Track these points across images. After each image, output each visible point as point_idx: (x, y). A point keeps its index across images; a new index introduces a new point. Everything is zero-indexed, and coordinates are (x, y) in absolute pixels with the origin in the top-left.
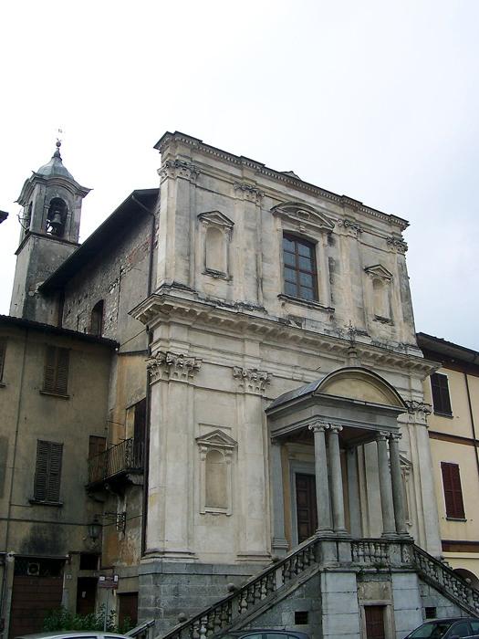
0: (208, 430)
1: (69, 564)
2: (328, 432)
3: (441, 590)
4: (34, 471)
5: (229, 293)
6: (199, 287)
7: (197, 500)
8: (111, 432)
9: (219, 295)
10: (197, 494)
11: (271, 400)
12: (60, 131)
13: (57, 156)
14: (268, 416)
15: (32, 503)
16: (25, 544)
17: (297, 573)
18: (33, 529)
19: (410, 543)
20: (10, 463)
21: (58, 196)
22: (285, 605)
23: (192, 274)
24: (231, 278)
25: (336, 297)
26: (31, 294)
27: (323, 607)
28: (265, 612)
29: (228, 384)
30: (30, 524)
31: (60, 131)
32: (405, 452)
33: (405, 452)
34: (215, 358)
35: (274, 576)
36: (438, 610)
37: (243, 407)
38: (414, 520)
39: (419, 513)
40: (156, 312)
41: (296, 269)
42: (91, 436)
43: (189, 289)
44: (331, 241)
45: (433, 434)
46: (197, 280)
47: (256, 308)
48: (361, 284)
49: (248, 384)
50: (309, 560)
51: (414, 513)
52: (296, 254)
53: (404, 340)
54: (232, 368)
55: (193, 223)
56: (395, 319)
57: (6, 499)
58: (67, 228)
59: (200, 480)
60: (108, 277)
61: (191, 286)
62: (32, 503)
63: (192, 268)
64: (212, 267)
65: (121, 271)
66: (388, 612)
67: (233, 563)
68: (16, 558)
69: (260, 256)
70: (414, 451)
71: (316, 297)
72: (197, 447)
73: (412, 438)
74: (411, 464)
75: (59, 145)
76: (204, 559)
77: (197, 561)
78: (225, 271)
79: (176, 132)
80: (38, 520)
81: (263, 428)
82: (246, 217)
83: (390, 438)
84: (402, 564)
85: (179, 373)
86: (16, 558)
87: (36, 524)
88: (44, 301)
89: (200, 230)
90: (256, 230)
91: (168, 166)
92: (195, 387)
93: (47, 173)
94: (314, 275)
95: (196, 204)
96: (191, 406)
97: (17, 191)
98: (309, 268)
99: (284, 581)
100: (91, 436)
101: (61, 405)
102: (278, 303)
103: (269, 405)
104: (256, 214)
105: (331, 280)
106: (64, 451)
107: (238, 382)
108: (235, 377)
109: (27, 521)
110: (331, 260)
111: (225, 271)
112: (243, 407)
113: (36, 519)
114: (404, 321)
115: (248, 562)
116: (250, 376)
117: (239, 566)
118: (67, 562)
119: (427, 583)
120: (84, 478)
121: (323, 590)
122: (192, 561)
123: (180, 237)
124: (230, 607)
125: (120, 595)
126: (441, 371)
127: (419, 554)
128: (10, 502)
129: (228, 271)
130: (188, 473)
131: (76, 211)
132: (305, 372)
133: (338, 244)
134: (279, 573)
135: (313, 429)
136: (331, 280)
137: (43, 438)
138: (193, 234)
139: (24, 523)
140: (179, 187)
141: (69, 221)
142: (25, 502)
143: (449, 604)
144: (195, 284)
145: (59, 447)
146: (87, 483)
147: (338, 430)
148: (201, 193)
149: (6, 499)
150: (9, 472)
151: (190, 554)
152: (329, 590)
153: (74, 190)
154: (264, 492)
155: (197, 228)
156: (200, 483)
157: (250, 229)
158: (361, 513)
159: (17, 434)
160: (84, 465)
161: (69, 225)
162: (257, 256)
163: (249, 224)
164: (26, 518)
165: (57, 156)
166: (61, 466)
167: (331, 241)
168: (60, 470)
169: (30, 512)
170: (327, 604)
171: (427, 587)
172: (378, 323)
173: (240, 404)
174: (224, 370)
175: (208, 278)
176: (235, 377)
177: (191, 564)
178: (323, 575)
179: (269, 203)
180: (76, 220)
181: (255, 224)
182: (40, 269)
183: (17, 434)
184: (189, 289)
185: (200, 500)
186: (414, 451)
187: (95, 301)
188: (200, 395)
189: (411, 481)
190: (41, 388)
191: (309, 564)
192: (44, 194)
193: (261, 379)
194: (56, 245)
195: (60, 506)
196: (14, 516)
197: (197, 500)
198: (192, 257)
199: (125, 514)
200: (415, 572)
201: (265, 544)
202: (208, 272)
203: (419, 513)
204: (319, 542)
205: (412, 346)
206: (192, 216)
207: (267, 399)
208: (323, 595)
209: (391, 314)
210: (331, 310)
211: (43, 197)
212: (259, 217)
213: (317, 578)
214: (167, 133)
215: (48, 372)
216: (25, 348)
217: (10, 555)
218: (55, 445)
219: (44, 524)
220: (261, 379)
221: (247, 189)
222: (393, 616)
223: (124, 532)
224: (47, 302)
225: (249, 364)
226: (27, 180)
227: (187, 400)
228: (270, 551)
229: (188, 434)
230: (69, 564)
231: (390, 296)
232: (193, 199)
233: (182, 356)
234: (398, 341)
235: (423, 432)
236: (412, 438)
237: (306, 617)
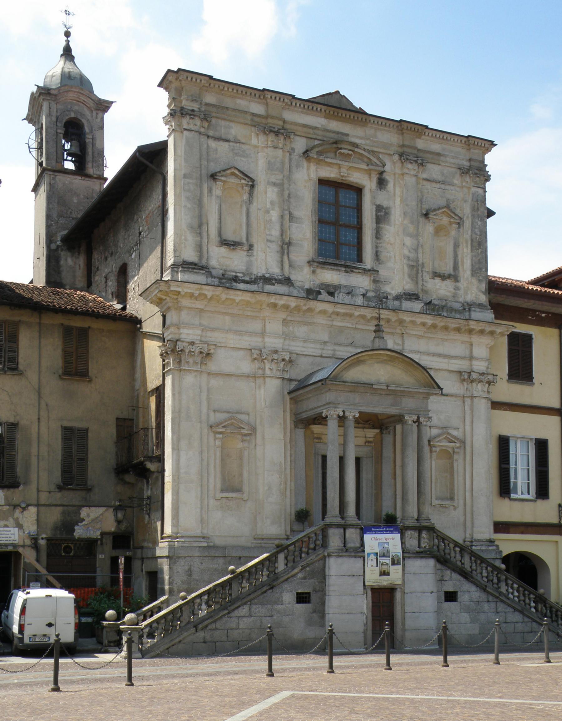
0: (221, 416)
1: (102, 544)
2: (342, 419)
3: (465, 575)
4: (59, 457)
5: (249, 265)
6: (213, 263)
7: (211, 487)
8: (137, 415)
9: (236, 269)
10: (212, 480)
11: (295, 380)
12: (67, 13)
13: (67, 53)
14: (291, 399)
15: (60, 488)
16: (56, 528)
17: (301, 557)
18: (63, 513)
19: (431, 529)
20: (34, 451)
21: (73, 115)
22: (286, 586)
23: (205, 248)
24: (251, 247)
25: (382, 256)
26: (53, 246)
27: (327, 588)
28: (265, 592)
29: (246, 367)
30: (60, 509)
31: (67, 13)
32: (456, 428)
33: (456, 428)
34: (233, 340)
35: (276, 561)
36: (459, 594)
37: (262, 391)
38: (461, 502)
39: (468, 494)
40: (164, 297)
41: (336, 224)
42: (117, 419)
43: (202, 268)
44: (382, 183)
45: (496, 405)
46: (211, 254)
47: (279, 282)
48: (416, 236)
49: (268, 366)
50: (309, 549)
51: (461, 492)
52: (337, 204)
53: (470, 298)
54: (251, 350)
55: (205, 186)
56: (461, 274)
57: (34, 486)
58: (89, 158)
59: (215, 467)
60: (129, 236)
61: (204, 262)
62: (60, 488)
63: (205, 240)
64: (230, 236)
65: (140, 233)
66: (398, 595)
67: (249, 545)
68: (48, 539)
69: (287, 217)
70: (468, 428)
71: (360, 259)
72: (212, 435)
73: (468, 412)
74: (463, 442)
75: (67, 34)
76: (218, 542)
77: (211, 544)
78: (244, 240)
79: (179, 70)
80: (67, 504)
81: (284, 411)
82: (270, 166)
83: (418, 421)
84: (418, 549)
85: (191, 360)
86: (48, 539)
87: (65, 508)
88: (69, 254)
89: (214, 193)
90: (282, 184)
91: (172, 114)
92: (209, 374)
93: (55, 83)
94: (359, 228)
95: (208, 161)
96: (204, 396)
97: (24, 109)
98: (354, 221)
99: (286, 565)
100: (117, 419)
101: (81, 388)
102: (307, 270)
103: (293, 385)
104: (283, 163)
105: (378, 235)
106: (90, 434)
107: (257, 364)
108: (255, 359)
109: (56, 505)
110: (379, 208)
111: (244, 240)
112: (262, 391)
113: (65, 503)
114: (473, 275)
115: (263, 545)
116: (270, 358)
117: (255, 547)
118: (99, 542)
119: (449, 568)
120: (112, 461)
121: (327, 573)
122: (205, 544)
123: (189, 206)
124: (231, 588)
125: (95, 586)
126: (521, 328)
127: (444, 539)
128: (38, 489)
129: (247, 239)
130: (202, 460)
131: (97, 134)
132: (337, 348)
133: (390, 186)
134: (281, 557)
135: (327, 417)
136: (378, 235)
137: (66, 424)
138: (205, 200)
139: (53, 508)
140: (187, 142)
141: (90, 150)
142: (53, 487)
143: (473, 588)
144: (208, 259)
145: (83, 433)
146: (115, 467)
147: (354, 417)
148: (213, 144)
149: (34, 486)
150: (34, 460)
151: (204, 538)
152: (331, 574)
153: (91, 104)
154: (283, 477)
155: (210, 190)
156: (215, 471)
157: (274, 184)
158: (396, 495)
159: (39, 422)
160: (111, 447)
161: (90, 153)
162: (282, 217)
163: (273, 179)
164: (54, 503)
165: (67, 53)
166: (87, 450)
167: (382, 183)
168: (87, 454)
169: (58, 496)
170: (329, 586)
171: (448, 572)
172: (438, 280)
173: (260, 387)
174: (242, 353)
175: (224, 250)
176: (255, 359)
177: (204, 547)
178: (327, 559)
179: (300, 144)
180: (98, 145)
181: (281, 177)
182: (60, 216)
183: (39, 422)
184: (202, 268)
185: (215, 486)
186: (468, 428)
187: (120, 264)
188: (214, 382)
189: (461, 461)
190: (60, 372)
191: (314, 549)
192: (54, 114)
193: (283, 360)
194: (78, 181)
195: (89, 490)
196: (42, 502)
197: (211, 487)
198: (204, 227)
199: (149, 498)
200: (432, 557)
201: (283, 528)
202: (225, 243)
203: (468, 494)
204: (326, 528)
205: (480, 306)
206: (204, 172)
207: (290, 380)
208: (327, 577)
209: (456, 267)
210: (373, 271)
211: (54, 119)
212: (287, 166)
213: (321, 562)
214: (169, 71)
215: (66, 355)
216: (40, 332)
217: (42, 539)
218: (79, 430)
219: (74, 508)
220: (283, 360)
221: (271, 131)
222: (403, 599)
223: (149, 516)
224: (72, 256)
225: (272, 342)
226: (32, 94)
227: (200, 387)
228: (288, 533)
229: (201, 422)
230: (102, 544)
231: (456, 246)
232: (205, 156)
233: (192, 343)
234: (461, 300)
235: (483, 406)
236: (468, 412)
237: (309, 597)
